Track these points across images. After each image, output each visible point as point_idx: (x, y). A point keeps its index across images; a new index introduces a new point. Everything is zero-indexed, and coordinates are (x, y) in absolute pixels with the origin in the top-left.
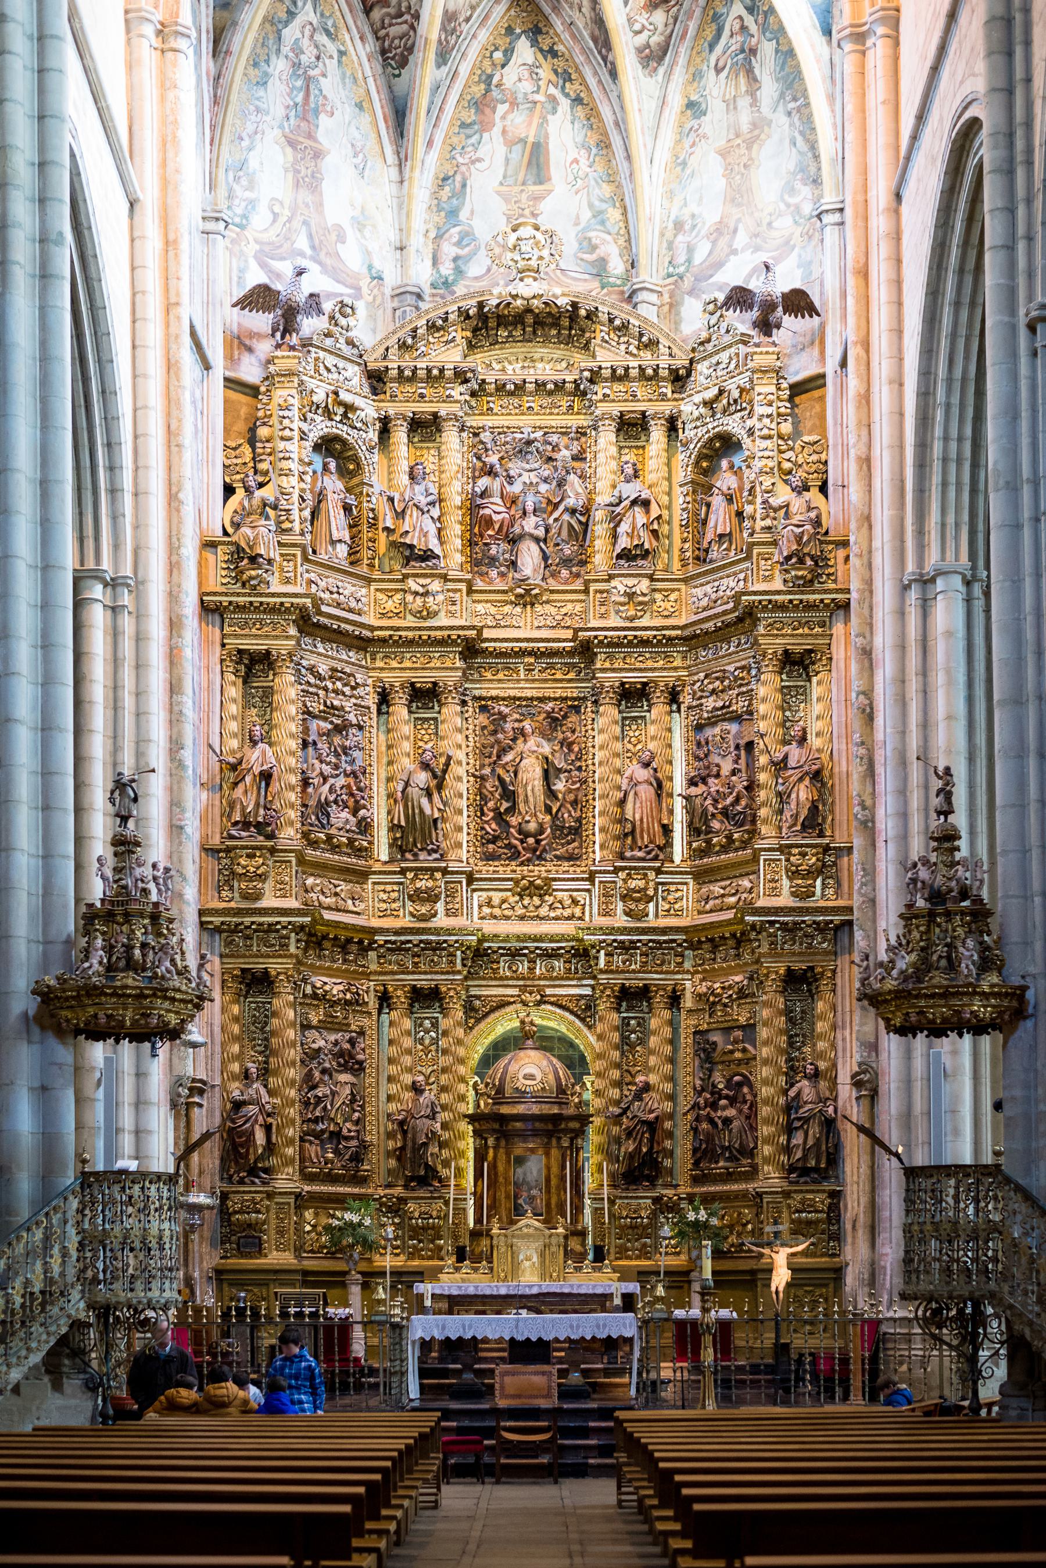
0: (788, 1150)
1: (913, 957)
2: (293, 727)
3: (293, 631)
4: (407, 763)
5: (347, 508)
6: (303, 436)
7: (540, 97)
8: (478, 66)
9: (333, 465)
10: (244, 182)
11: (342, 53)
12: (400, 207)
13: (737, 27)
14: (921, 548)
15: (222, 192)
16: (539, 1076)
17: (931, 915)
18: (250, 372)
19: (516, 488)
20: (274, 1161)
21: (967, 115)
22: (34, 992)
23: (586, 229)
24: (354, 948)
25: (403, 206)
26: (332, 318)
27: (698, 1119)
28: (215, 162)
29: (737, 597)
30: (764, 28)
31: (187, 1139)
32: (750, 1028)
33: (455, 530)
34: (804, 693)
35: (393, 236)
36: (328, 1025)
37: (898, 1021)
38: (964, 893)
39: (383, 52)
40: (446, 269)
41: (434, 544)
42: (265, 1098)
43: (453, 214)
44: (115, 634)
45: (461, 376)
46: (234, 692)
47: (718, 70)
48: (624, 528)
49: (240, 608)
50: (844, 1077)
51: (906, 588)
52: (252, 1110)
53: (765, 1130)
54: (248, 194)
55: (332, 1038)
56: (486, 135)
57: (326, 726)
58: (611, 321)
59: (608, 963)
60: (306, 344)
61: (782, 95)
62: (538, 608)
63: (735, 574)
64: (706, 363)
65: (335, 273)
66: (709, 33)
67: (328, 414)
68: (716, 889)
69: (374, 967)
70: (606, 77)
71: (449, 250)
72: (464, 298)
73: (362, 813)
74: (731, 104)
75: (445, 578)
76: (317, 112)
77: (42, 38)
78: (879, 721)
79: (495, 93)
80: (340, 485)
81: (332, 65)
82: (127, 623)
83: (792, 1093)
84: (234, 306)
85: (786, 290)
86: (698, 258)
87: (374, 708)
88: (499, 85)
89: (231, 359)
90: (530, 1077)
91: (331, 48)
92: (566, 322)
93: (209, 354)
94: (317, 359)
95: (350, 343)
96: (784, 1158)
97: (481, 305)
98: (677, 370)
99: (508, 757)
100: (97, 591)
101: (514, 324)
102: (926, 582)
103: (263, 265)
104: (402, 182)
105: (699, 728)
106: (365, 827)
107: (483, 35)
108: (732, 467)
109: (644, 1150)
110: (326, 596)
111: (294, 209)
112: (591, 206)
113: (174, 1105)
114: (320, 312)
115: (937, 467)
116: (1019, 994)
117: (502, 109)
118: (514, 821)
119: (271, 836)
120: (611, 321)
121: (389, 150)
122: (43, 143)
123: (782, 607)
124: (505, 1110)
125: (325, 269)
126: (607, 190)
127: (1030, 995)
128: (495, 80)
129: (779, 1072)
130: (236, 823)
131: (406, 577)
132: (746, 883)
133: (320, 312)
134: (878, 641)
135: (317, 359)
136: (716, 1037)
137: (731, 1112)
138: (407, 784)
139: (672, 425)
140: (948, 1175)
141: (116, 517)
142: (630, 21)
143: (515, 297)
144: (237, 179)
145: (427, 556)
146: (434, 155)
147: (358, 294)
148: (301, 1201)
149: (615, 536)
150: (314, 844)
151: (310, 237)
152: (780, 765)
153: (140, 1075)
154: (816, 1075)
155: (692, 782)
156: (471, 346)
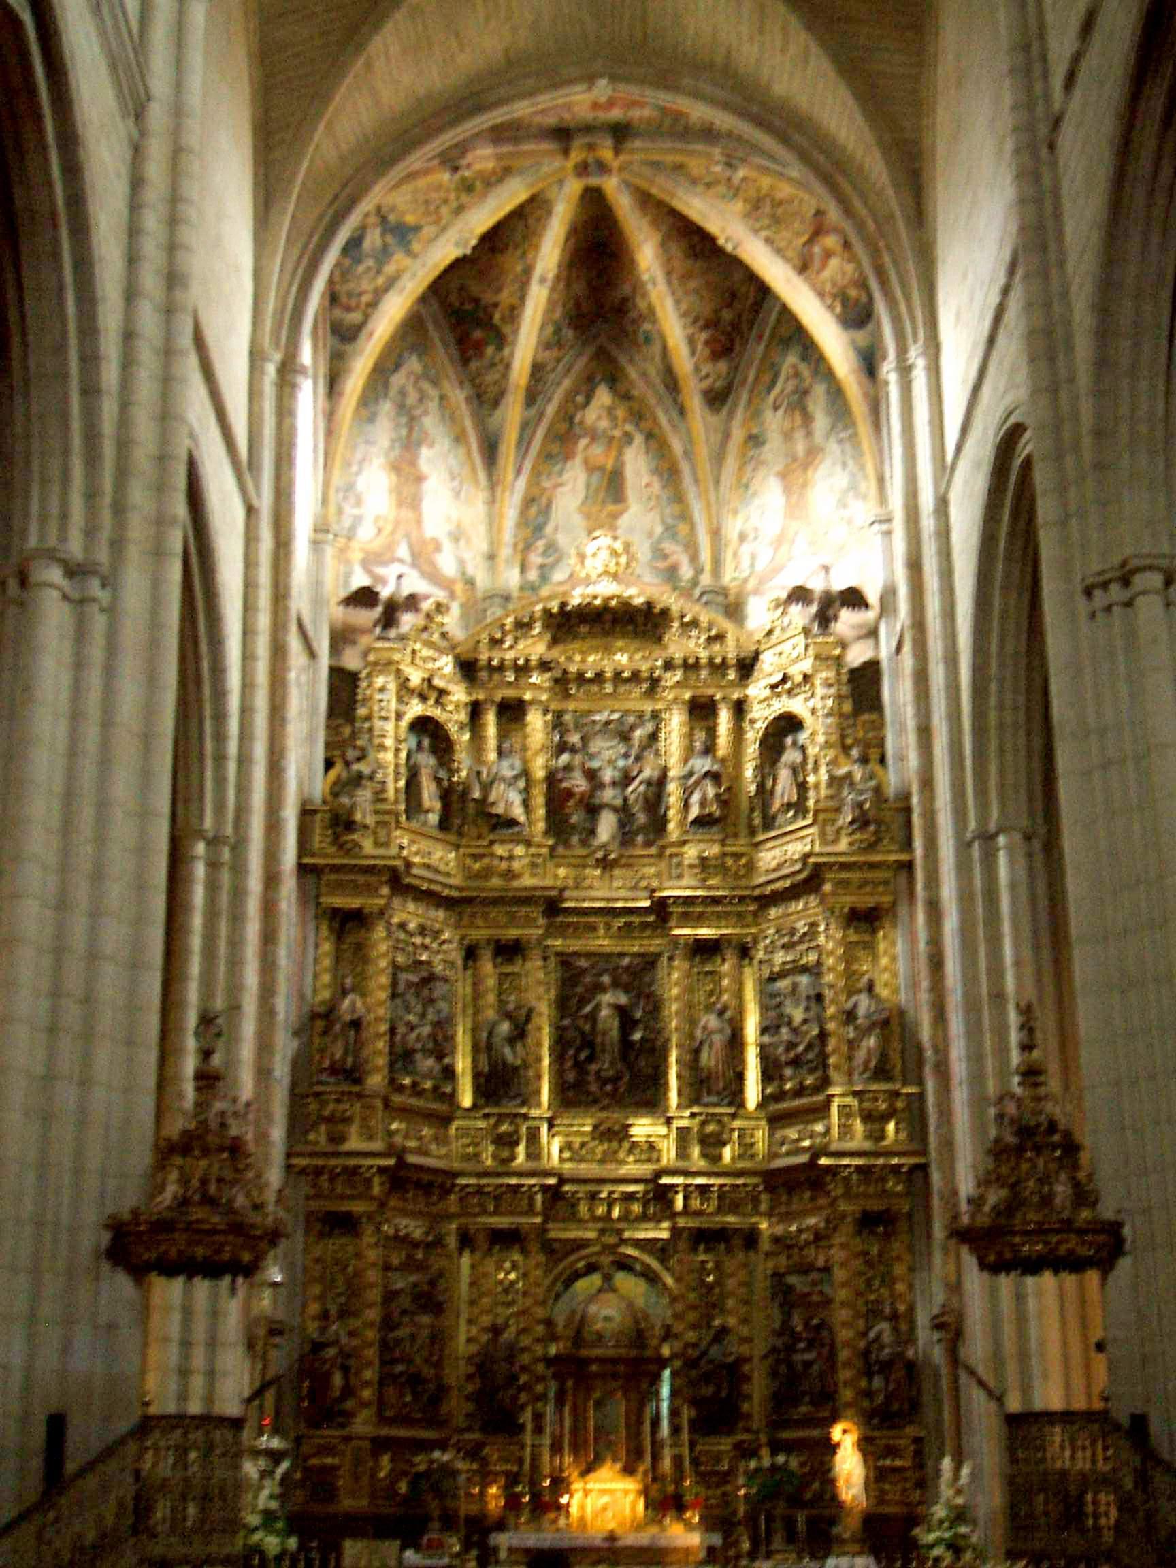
0: (869, 1394)
1: (1004, 1193)
2: (384, 980)
3: (385, 891)
4: (490, 1014)
5: (438, 780)
6: (399, 716)
7: (617, 433)
8: (562, 408)
9: (426, 742)
10: (352, 500)
11: (442, 398)
13: (791, 371)
15: (332, 509)
16: (618, 1318)
17: (1020, 1149)
18: (351, 660)
19: (595, 764)
20: (349, 1404)
21: (1012, 420)
22: (107, 1227)
23: (660, 541)
24: (436, 1191)
25: (493, 522)
26: (429, 616)
27: (778, 1361)
28: (326, 484)
29: (806, 857)
30: (815, 373)
31: (972, 1373)
32: (827, 1269)
33: (539, 800)
34: (870, 947)
35: (484, 547)
36: (410, 1265)
37: (992, 1258)
38: (1052, 1127)
39: (479, 396)
40: (533, 575)
41: (518, 812)
42: (344, 1340)
43: (539, 529)
44: (212, 887)
45: (544, 666)
46: (327, 947)
47: (776, 408)
48: (696, 798)
49: (336, 869)
50: (922, 1319)
51: (969, 845)
52: (332, 1352)
53: (845, 1375)
54: (356, 512)
55: (413, 1278)
56: (569, 465)
57: (414, 978)
59: (685, 1206)
60: (402, 638)
61: (833, 427)
62: (617, 872)
63: (803, 838)
64: (771, 651)
65: (433, 576)
66: (767, 378)
67: (423, 698)
68: (792, 1134)
69: (453, 1209)
70: (675, 414)
71: (535, 559)
72: (550, 598)
73: (447, 1060)
74: (788, 436)
75: (528, 844)
76: (419, 444)
77: (168, 352)
79: (577, 430)
80: (432, 761)
81: (433, 405)
82: (225, 877)
83: (872, 1335)
86: (760, 566)
87: (460, 963)
88: (581, 422)
89: (335, 649)
90: (607, 1319)
91: (433, 392)
92: (640, 620)
93: (315, 645)
94: (414, 652)
95: (444, 635)
96: (866, 1403)
97: (563, 605)
99: (588, 1009)
100: (200, 848)
101: (594, 621)
102: (987, 838)
103: (369, 572)
105: (772, 979)
106: (449, 1073)
107: (567, 383)
108: (795, 743)
109: (724, 1394)
110: (416, 859)
111: (397, 524)
112: (663, 522)
113: (250, 1345)
114: (417, 610)
115: (993, 733)
116: (1113, 1229)
117: (583, 442)
118: (593, 1067)
119: (358, 1081)
121: (482, 475)
122: (165, 438)
123: (844, 866)
124: (584, 1352)
125: (424, 574)
127: (1127, 1231)
128: (577, 420)
129: (857, 1315)
130: (322, 1070)
131: (492, 843)
132: (819, 1128)
133: (417, 610)
135: (414, 652)
136: (792, 1280)
137: (809, 1356)
138: (490, 1034)
139: (740, 708)
140: (1052, 1424)
141: (220, 781)
142: (697, 369)
143: (595, 597)
144: (345, 498)
145: (512, 823)
146: (521, 483)
147: (452, 595)
148: (380, 1445)
149: (686, 806)
150: (401, 1089)
151: (411, 547)
152: (850, 1016)
153: (215, 1314)
154: (894, 1317)
155: (764, 1030)
156: (554, 641)
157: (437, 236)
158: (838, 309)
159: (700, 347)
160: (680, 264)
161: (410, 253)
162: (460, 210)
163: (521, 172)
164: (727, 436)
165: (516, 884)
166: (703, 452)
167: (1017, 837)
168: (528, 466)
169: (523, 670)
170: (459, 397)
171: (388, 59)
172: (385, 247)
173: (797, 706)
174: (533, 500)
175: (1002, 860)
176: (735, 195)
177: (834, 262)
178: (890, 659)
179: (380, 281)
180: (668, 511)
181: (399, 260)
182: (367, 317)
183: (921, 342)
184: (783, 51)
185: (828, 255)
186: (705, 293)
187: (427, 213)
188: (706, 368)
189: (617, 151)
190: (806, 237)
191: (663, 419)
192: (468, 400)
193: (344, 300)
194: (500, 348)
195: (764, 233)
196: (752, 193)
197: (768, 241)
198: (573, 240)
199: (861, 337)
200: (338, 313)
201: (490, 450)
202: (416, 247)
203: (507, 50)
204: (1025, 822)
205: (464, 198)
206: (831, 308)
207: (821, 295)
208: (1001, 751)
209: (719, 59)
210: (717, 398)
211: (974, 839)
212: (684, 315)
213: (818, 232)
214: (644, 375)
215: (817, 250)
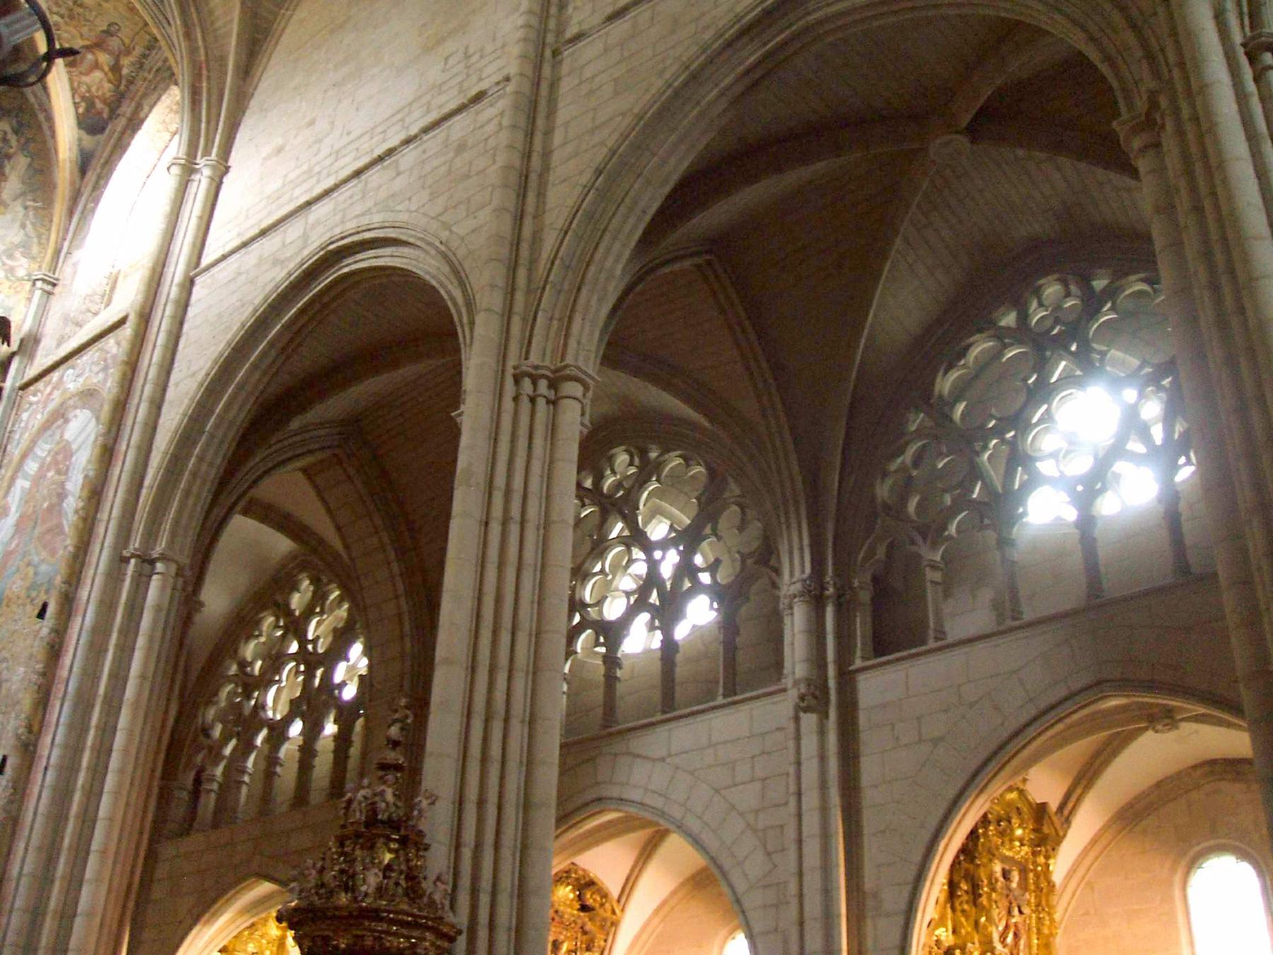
14: (151, 534)
51: (126, 560)
61: (23, 194)
78: (67, 660)
102: (147, 561)
134: (84, 593)
158: (81, 110)
165: (438, 264)
167: (173, 568)
175: (155, 582)
177: (98, 75)
178: (13, 389)
183: (213, 156)
185: (96, 66)
199: (89, 141)
204: (185, 560)
206: (76, 105)
207: (74, 91)
208: (187, 493)
211: (133, 556)
215: (90, 56)
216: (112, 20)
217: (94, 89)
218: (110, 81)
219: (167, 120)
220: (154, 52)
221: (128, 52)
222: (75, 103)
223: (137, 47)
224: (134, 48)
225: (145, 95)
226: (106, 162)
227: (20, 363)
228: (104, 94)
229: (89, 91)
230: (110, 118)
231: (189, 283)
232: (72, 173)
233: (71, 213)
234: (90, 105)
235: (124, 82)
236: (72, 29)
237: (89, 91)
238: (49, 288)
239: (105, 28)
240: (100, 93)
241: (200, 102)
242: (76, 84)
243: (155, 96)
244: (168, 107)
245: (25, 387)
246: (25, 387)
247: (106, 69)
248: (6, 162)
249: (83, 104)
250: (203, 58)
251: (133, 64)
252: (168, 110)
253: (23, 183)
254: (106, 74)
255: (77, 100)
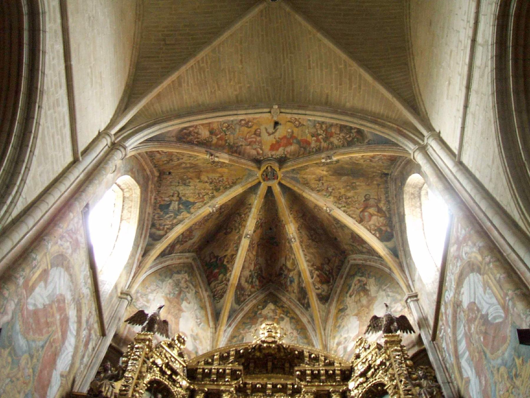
12: (213, 341)
58: (310, 355)
67: (163, 373)
84: (126, 321)
85: (398, 316)
98: (345, 371)
104: (216, 332)
107: (254, 302)
120: (310, 355)
121: (211, 324)
126: (305, 341)
146: (230, 330)
157: (202, 206)
158: (378, 235)
159: (315, 276)
160: (305, 238)
161: (189, 212)
162: (213, 197)
163: (239, 183)
164: (329, 312)
166: (318, 321)
168: (233, 325)
169: (221, 376)
170: (205, 295)
171: (188, 85)
172: (179, 208)
173: (381, 377)
174: (235, 337)
176: (330, 195)
177: (374, 218)
179: (175, 221)
180: (301, 341)
181: (185, 214)
182: (166, 233)
184: (350, 88)
185: (371, 215)
186: (317, 255)
187: (199, 197)
188: (318, 285)
189: (280, 169)
190: (361, 210)
191: (298, 312)
192: (208, 296)
193: (158, 226)
194: (225, 275)
195: (343, 209)
196: (337, 194)
197: (344, 211)
198: (259, 231)
200: (154, 230)
201: (217, 316)
202: (192, 210)
203: (237, 97)
205: (215, 193)
206: (374, 235)
207: (370, 230)
209: (323, 100)
210: (324, 299)
212: (308, 261)
213: (366, 207)
214: (290, 299)
215: (366, 214)
216: (364, 195)
217: (377, 224)
218: (381, 217)
219: (413, 203)
220: (389, 193)
221: (379, 200)
222: (373, 234)
223: (382, 197)
224: (381, 198)
225: (398, 209)
226: (403, 244)
227: (425, 332)
228: (382, 223)
229: (375, 226)
230: (392, 230)
231: (460, 164)
232: (391, 258)
233: (403, 271)
234: (379, 230)
235: (387, 213)
236: (352, 208)
237: (375, 226)
238: (415, 299)
239: (364, 199)
240: (381, 224)
241: (405, 133)
242: (368, 227)
243: (401, 204)
244: (409, 199)
245: (434, 337)
246: (434, 337)
247: (376, 213)
248: (366, 286)
249: (377, 232)
250: (396, 126)
251: (384, 204)
252: (410, 200)
253: (377, 285)
254: (378, 216)
255: (373, 232)
